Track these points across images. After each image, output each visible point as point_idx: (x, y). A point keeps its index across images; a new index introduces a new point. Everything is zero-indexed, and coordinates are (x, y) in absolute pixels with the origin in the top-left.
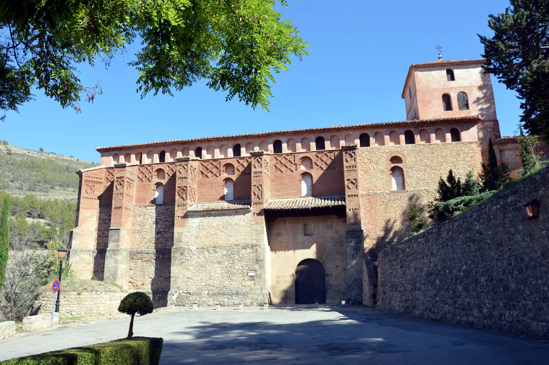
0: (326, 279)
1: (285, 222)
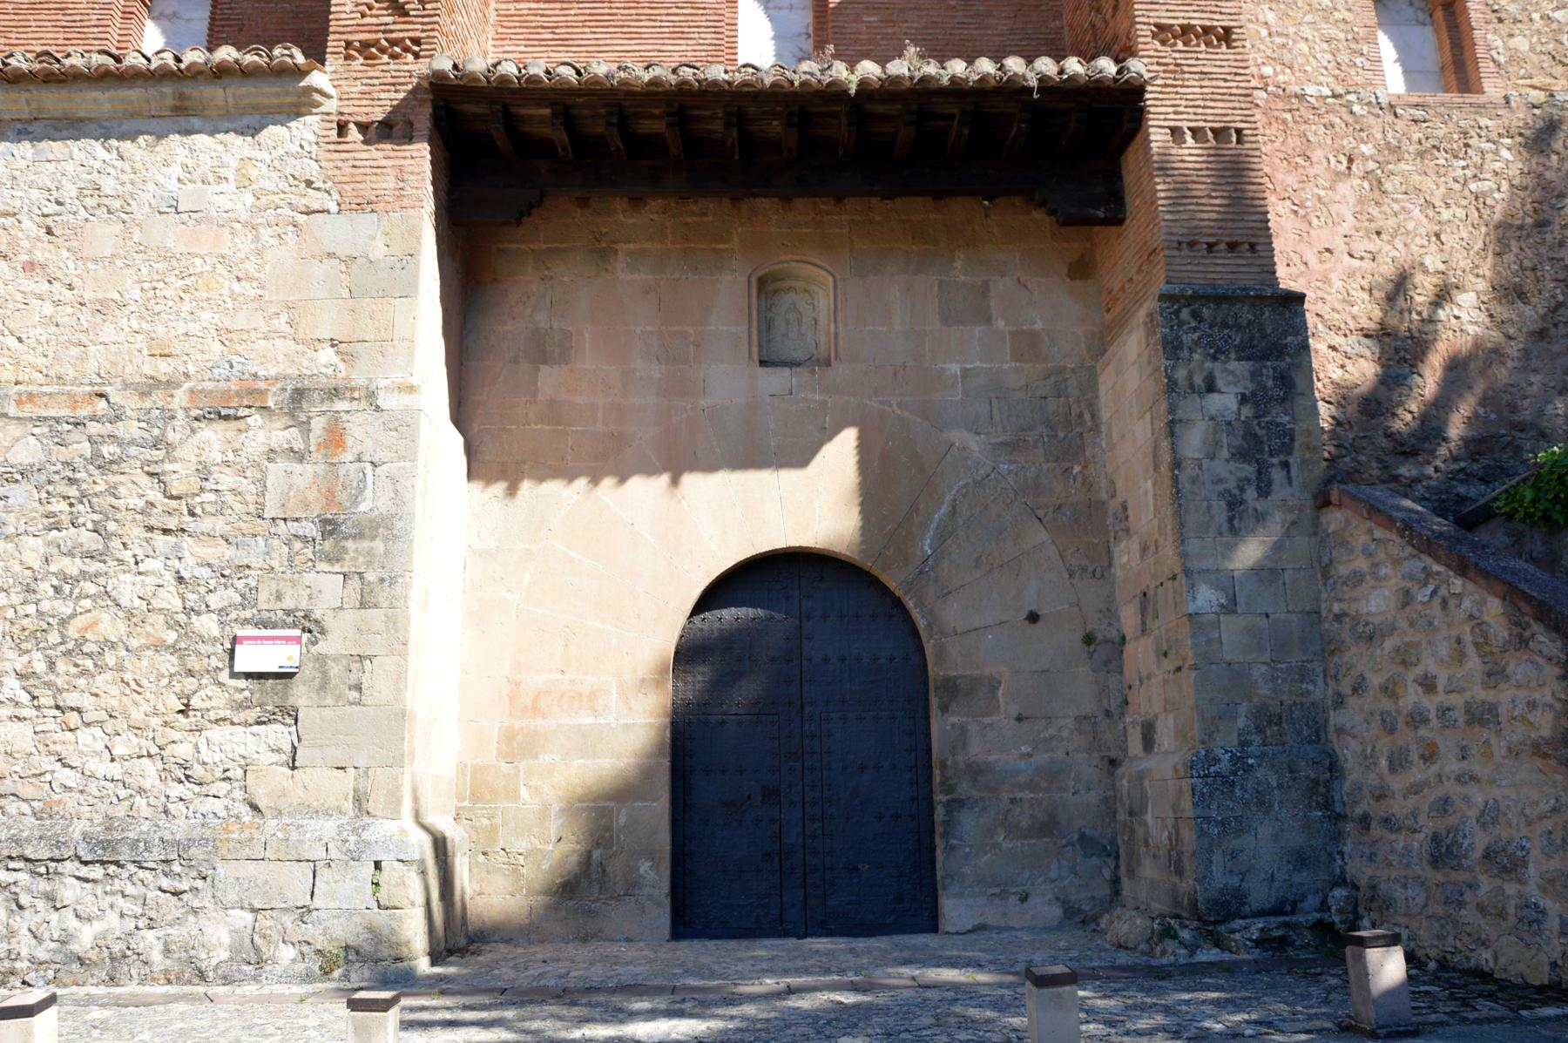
0: (941, 726)
1: (602, 252)
